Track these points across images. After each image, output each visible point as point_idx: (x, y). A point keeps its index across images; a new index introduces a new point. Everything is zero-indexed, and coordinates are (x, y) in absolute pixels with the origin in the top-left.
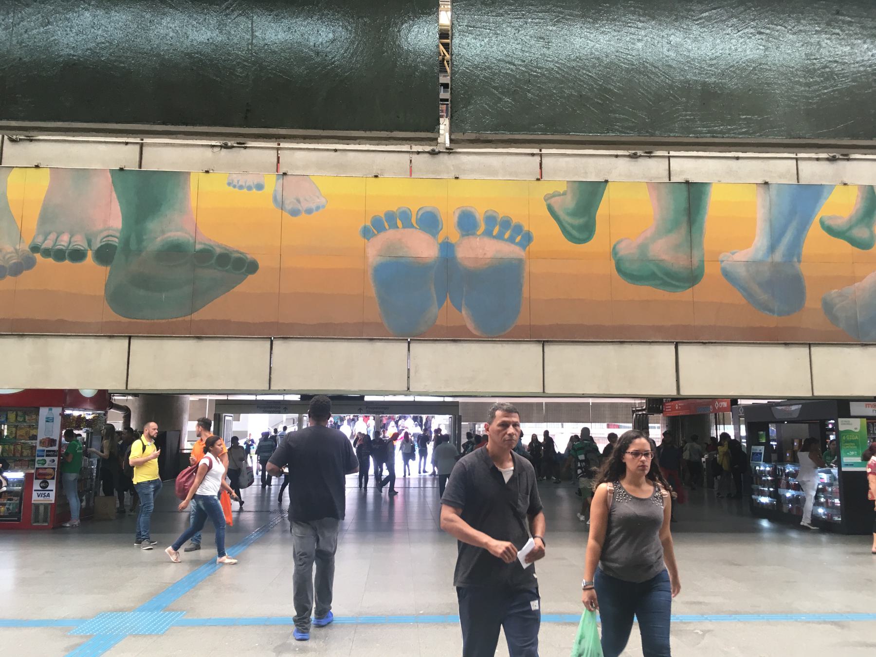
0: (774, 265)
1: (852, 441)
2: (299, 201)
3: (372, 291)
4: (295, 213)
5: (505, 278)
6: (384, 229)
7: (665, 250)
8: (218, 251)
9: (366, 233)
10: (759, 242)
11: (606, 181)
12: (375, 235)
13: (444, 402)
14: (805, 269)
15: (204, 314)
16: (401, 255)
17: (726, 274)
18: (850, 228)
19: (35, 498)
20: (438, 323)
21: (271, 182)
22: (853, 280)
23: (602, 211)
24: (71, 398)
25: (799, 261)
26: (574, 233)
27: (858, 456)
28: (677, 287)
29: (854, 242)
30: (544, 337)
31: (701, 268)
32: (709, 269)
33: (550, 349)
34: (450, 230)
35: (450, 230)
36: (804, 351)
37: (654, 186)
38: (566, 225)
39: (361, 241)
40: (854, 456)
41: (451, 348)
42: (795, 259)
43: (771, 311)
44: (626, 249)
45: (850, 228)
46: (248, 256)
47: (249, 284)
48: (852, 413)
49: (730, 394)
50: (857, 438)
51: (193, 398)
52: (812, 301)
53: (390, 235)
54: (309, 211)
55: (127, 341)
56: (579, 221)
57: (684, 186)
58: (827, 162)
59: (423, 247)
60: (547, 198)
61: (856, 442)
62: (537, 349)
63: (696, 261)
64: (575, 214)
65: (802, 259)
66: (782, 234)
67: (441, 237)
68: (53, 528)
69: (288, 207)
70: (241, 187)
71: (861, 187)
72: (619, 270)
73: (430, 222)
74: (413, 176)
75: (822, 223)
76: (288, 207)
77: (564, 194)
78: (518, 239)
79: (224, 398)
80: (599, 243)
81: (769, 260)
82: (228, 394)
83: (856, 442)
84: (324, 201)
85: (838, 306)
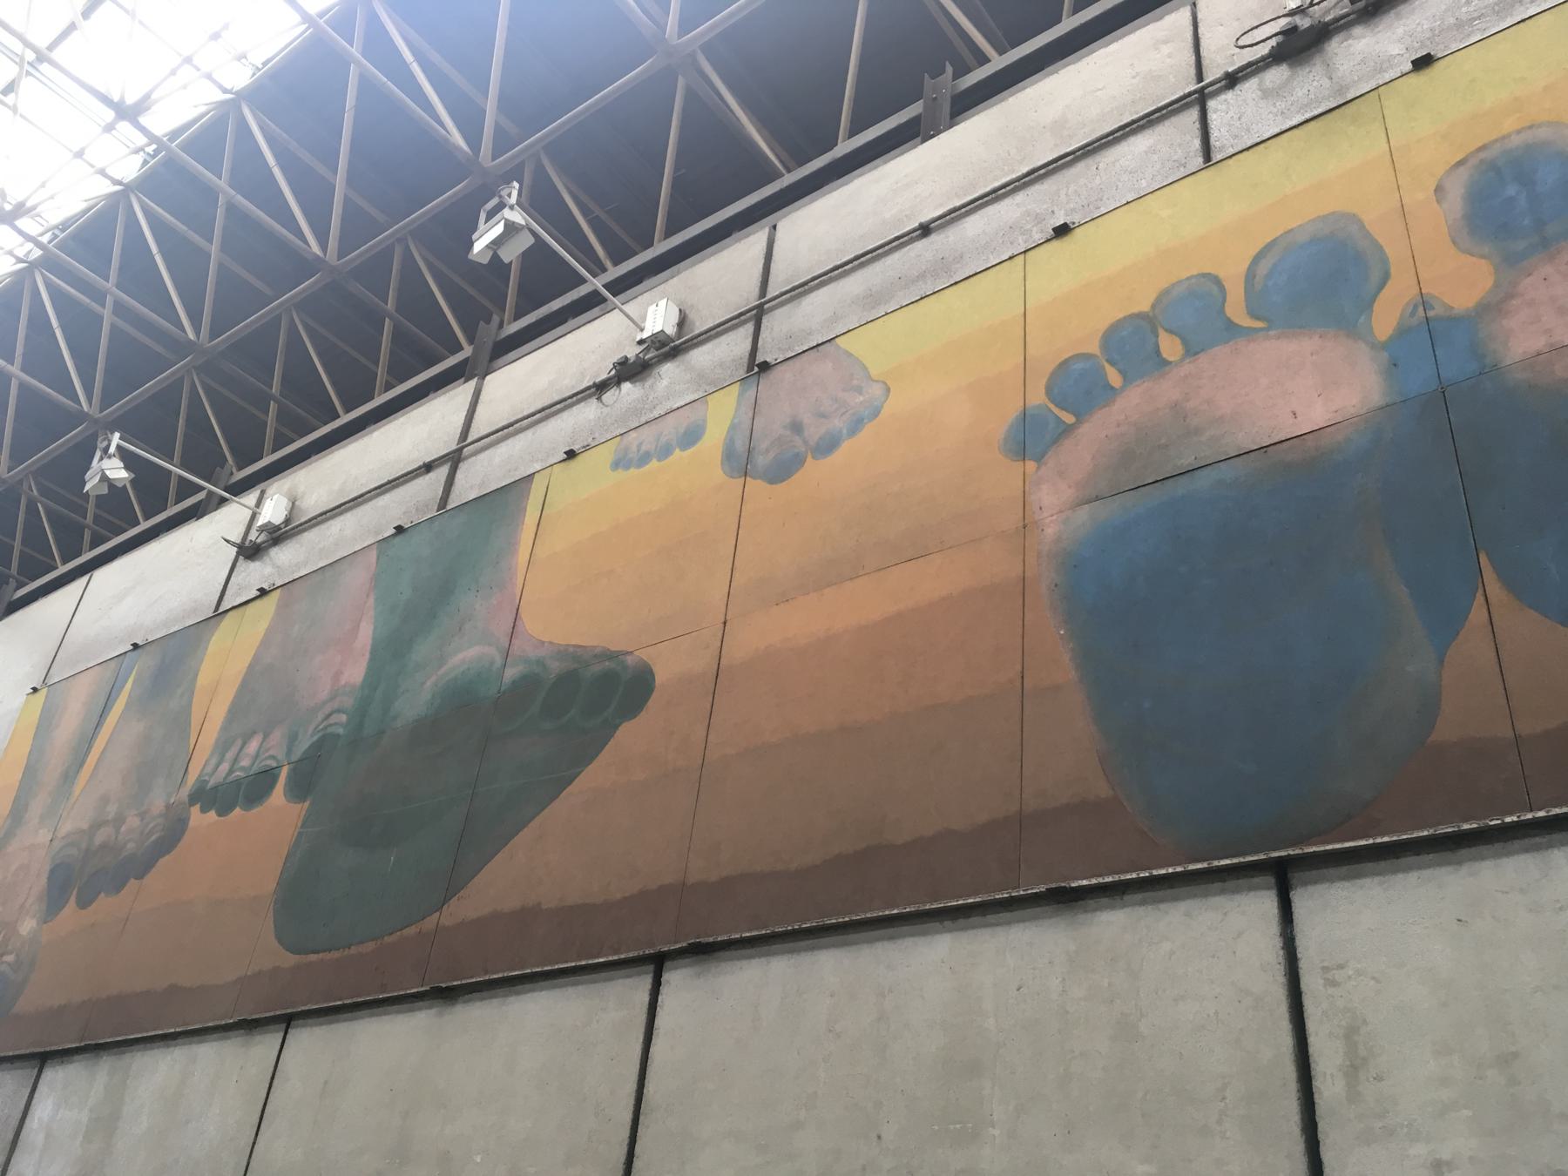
3: (1058, 662)
4: (782, 471)
6: (1110, 392)
12: (1068, 430)
15: (498, 886)
16: (1187, 461)
18: (1288, 81)
20: (1446, 730)
39: (1008, 476)
46: (629, 660)
53: (1133, 404)
55: (646, 982)
67: (1386, 318)
74: (1217, 157)
84: (876, 390)
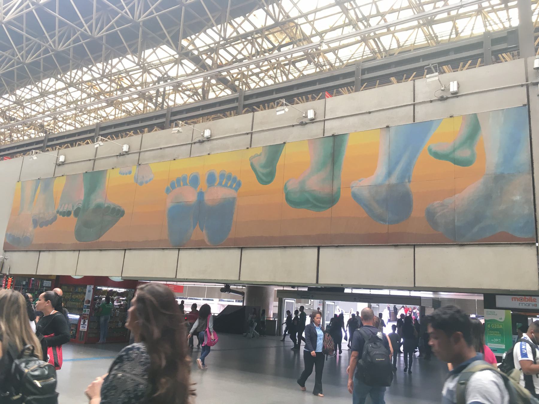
0: (391, 187)
1: (497, 330)
2: (143, 177)
5: (226, 209)
7: (316, 183)
8: (112, 206)
9: (168, 191)
10: (381, 170)
11: (285, 143)
13: (370, 294)
14: (413, 187)
17: (355, 196)
18: (454, 151)
19: (81, 329)
21: (134, 169)
22: (454, 192)
23: (281, 162)
24: (105, 280)
25: (409, 182)
26: (264, 178)
27: (502, 342)
28: (320, 207)
29: (457, 162)
30: (242, 245)
31: (338, 192)
32: (345, 194)
33: (246, 253)
34: (203, 183)
35: (203, 183)
36: (410, 250)
37: (312, 141)
38: (260, 174)
40: (498, 343)
41: (197, 253)
42: (407, 181)
43: (384, 221)
44: (293, 186)
45: (454, 151)
47: (122, 222)
48: (498, 305)
49: (352, 283)
50: (501, 327)
51: (276, 288)
52: (418, 211)
54: (147, 182)
56: (268, 170)
57: (332, 138)
58: (440, 102)
59: (190, 196)
60: (251, 158)
61: (500, 331)
62: (237, 252)
63: (335, 188)
64: (264, 167)
65: (411, 179)
66: (397, 163)
68: (85, 343)
69: (139, 181)
70: (126, 174)
71: (464, 117)
72: (288, 200)
73: (195, 181)
75: (430, 150)
76: (139, 181)
77: (260, 155)
78: (234, 186)
79: (281, 288)
80: (277, 184)
81: (387, 183)
82: (283, 286)
83: (500, 331)
85: (439, 214)
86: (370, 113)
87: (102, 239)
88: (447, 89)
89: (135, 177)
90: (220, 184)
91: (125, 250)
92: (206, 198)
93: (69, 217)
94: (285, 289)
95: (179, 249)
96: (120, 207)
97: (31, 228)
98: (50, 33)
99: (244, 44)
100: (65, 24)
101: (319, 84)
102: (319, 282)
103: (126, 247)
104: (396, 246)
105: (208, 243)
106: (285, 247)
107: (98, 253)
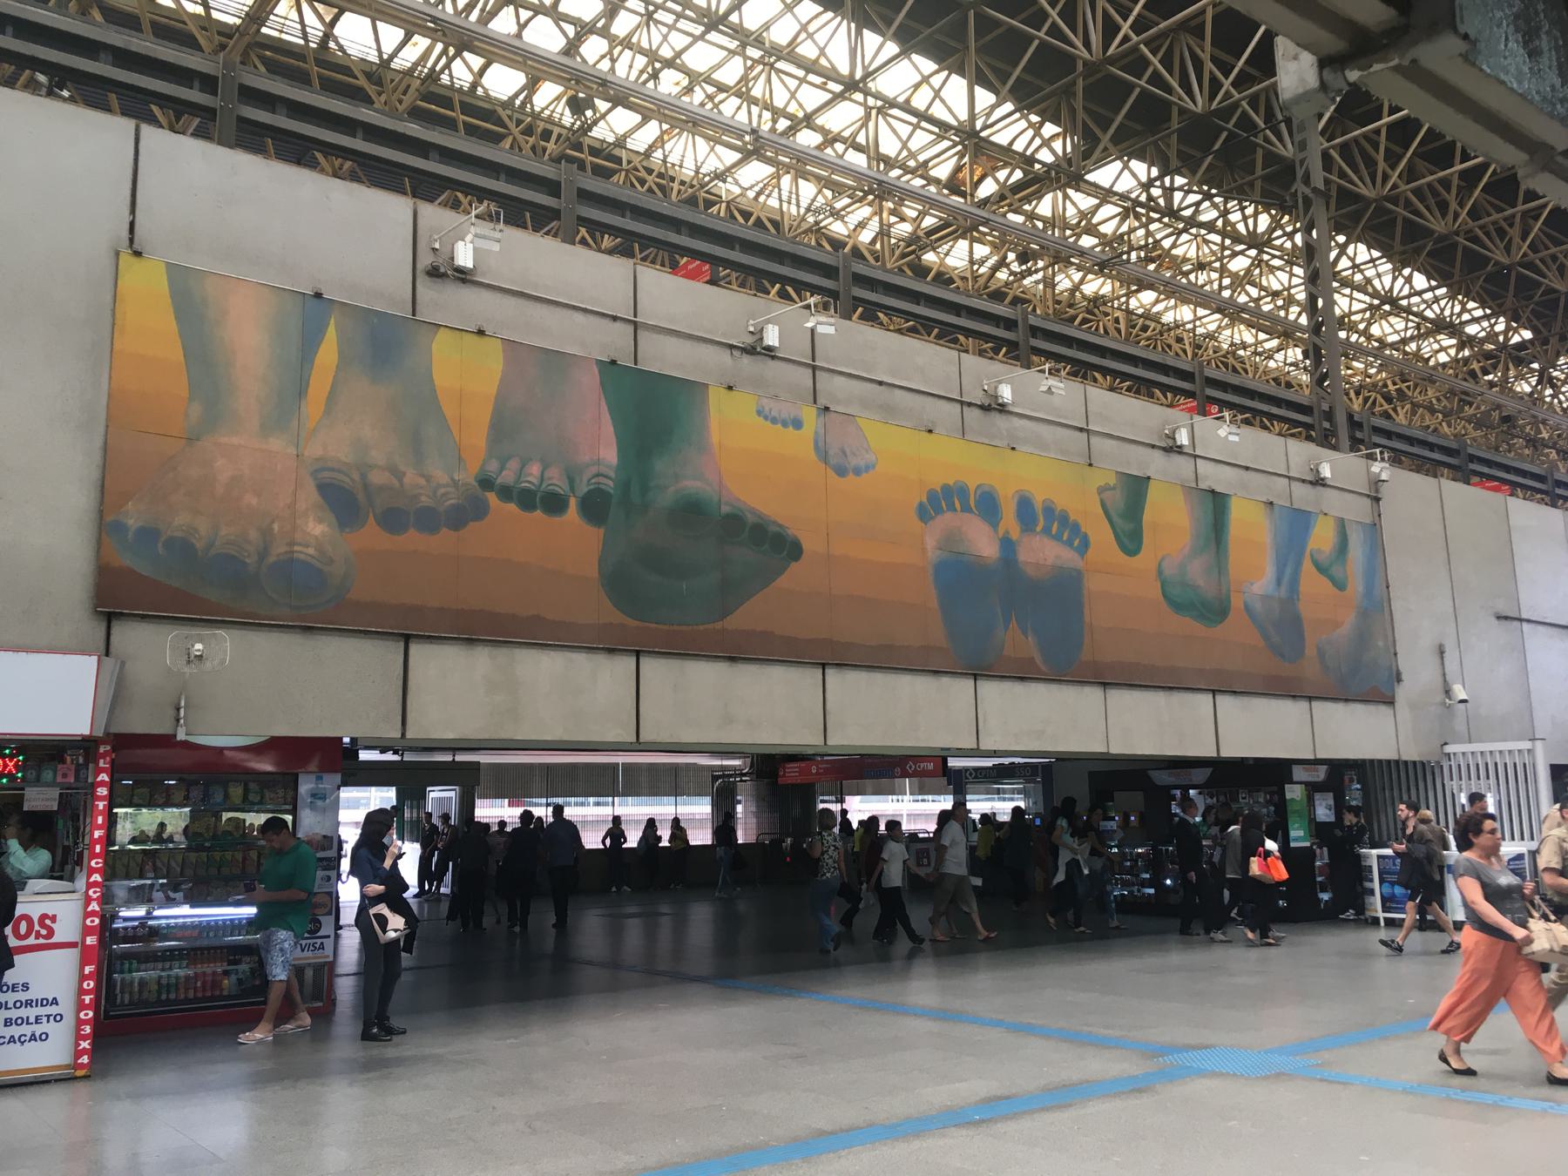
32: (1236, 602)
41: (1018, 688)
47: (794, 577)
86: (1247, 468)
87: (735, 622)
88: (759, 333)
89: (816, 442)
90: (1047, 531)
91: (824, 666)
92: (1023, 556)
93: (557, 519)
94: (408, 757)
95: (975, 677)
96: (780, 526)
97: (317, 527)
98: (1147, 14)
99: (909, 150)
100: (1199, 32)
101: (15, 36)
102: (409, 735)
103: (826, 656)
104: (732, 659)
105: (1043, 668)
106: (1171, 688)
107: (721, 668)
